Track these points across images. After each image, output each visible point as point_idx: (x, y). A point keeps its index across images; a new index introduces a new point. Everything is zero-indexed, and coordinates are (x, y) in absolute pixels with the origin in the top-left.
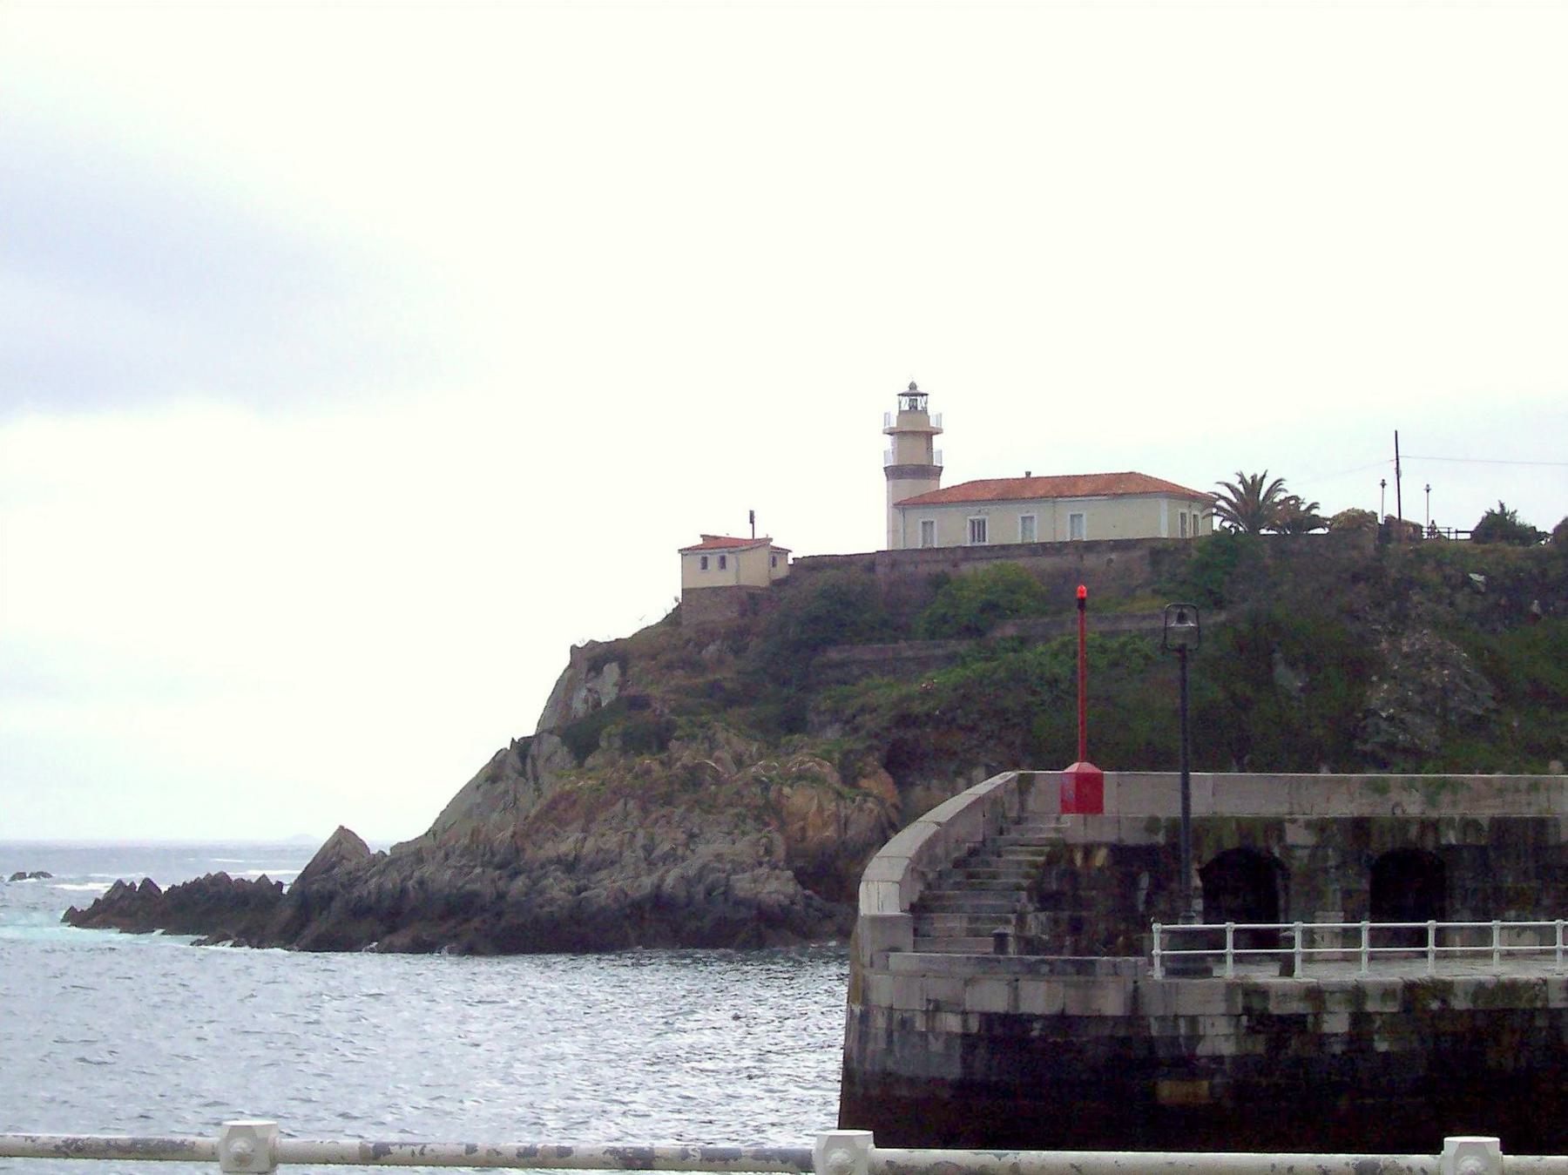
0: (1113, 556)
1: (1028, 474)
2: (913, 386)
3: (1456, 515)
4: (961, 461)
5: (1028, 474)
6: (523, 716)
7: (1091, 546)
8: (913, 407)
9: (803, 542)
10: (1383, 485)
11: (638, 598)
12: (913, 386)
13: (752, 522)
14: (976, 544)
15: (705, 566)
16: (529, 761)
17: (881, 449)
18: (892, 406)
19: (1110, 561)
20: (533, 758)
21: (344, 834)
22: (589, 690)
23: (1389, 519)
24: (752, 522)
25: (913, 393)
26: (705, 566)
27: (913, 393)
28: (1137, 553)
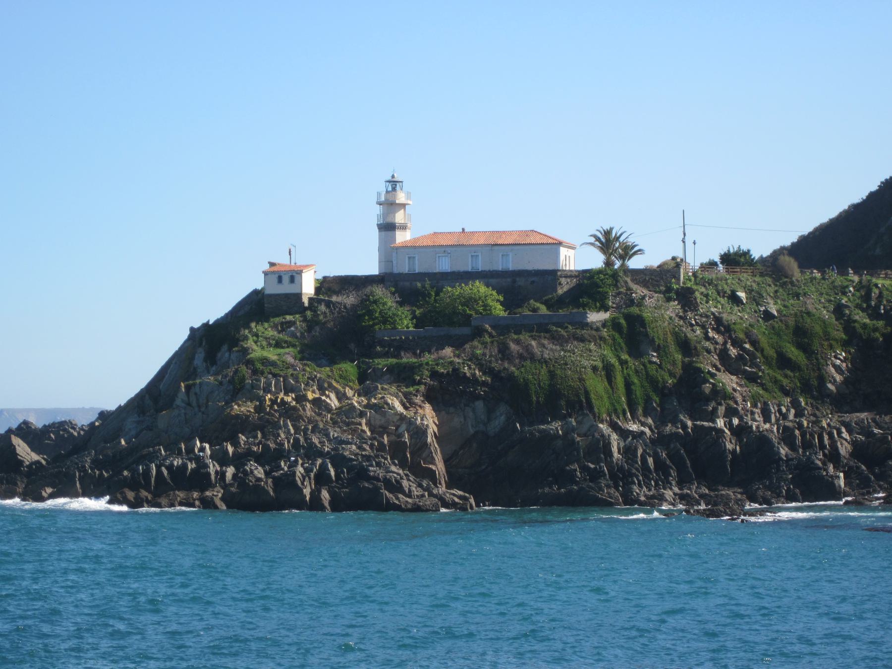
1: (463, 229)
5: (463, 229)
10: (694, 243)
12: (393, 177)
17: (374, 213)
20: (196, 394)
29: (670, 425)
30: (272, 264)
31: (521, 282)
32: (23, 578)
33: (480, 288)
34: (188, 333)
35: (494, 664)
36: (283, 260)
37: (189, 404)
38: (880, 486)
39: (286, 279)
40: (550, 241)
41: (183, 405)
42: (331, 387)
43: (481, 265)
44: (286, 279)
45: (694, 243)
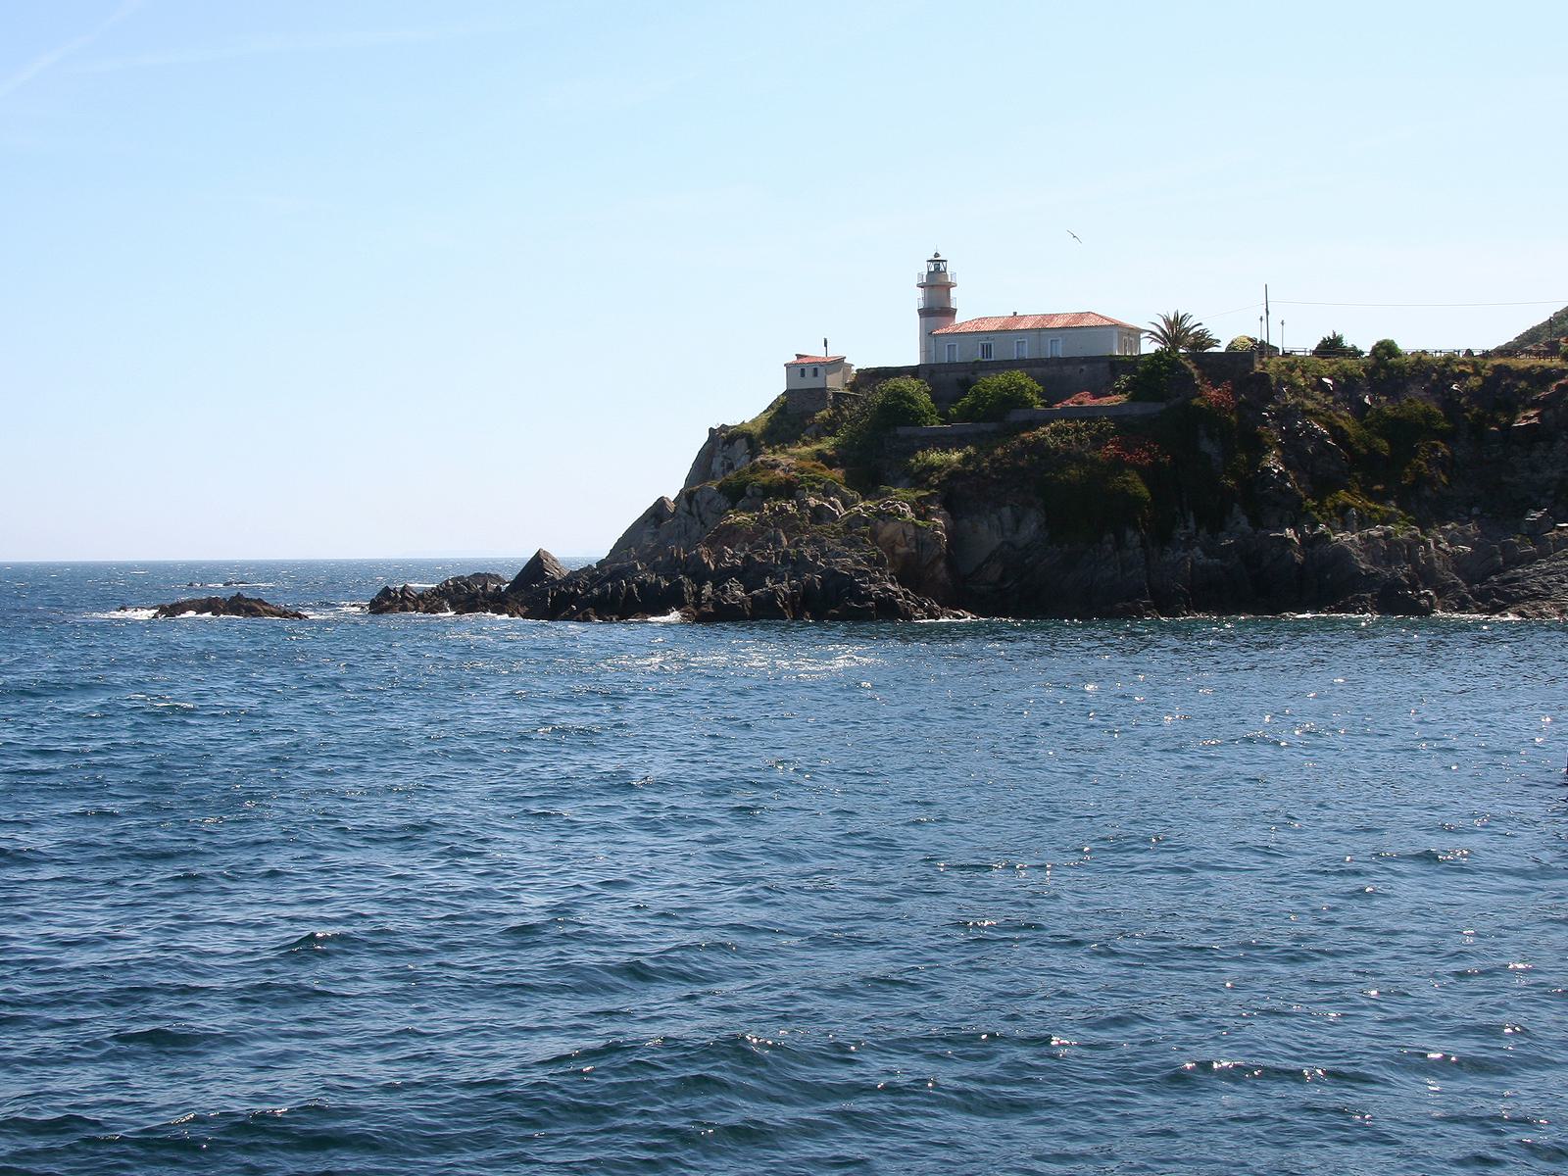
0: (1084, 367)
1: (1015, 313)
2: (937, 255)
3: (1298, 337)
4: (975, 305)
5: (1015, 313)
6: (671, 486)
7: (1068, 361)
8: (937, 269)
9: (863, 357)
10: (1283, 324)
11: (750, 400)
12: (937, 255)
13: (826, 345)
14: (986, 360)
15: (803, 375)
16: (694, 503)
17: (916, 298)
18: (924, 269)
19: (1082, 370)
20: (697, 501)
21: (711, 429)
22: (725, 457)
23: (1262, 342)
24: (826, 345)
25: (937, 261)
26: (803, 375)
27: (937, 261)
28: (1101, 365)
29: (920, 452)
30: (799, 356)
31: (1068, 370)
32: (1151, 920)
33: (1020, 377)
34: (705, 437)
35: (1545, 994)
36: (817, 352)
37: (690, 513)
38: (1478, 607)
39: (809, 372)
40: (1106, 323)
41: (685, 514)
42: (837, 492)
43: (1027, 353)
44: (809, 372)
45: (1283, 324)
